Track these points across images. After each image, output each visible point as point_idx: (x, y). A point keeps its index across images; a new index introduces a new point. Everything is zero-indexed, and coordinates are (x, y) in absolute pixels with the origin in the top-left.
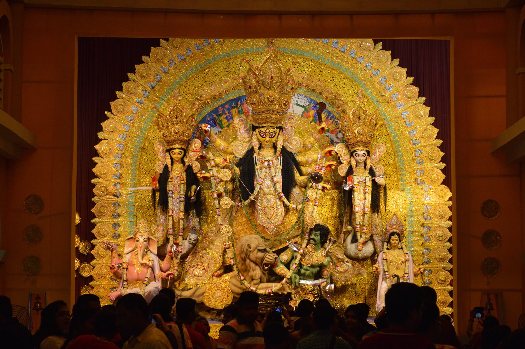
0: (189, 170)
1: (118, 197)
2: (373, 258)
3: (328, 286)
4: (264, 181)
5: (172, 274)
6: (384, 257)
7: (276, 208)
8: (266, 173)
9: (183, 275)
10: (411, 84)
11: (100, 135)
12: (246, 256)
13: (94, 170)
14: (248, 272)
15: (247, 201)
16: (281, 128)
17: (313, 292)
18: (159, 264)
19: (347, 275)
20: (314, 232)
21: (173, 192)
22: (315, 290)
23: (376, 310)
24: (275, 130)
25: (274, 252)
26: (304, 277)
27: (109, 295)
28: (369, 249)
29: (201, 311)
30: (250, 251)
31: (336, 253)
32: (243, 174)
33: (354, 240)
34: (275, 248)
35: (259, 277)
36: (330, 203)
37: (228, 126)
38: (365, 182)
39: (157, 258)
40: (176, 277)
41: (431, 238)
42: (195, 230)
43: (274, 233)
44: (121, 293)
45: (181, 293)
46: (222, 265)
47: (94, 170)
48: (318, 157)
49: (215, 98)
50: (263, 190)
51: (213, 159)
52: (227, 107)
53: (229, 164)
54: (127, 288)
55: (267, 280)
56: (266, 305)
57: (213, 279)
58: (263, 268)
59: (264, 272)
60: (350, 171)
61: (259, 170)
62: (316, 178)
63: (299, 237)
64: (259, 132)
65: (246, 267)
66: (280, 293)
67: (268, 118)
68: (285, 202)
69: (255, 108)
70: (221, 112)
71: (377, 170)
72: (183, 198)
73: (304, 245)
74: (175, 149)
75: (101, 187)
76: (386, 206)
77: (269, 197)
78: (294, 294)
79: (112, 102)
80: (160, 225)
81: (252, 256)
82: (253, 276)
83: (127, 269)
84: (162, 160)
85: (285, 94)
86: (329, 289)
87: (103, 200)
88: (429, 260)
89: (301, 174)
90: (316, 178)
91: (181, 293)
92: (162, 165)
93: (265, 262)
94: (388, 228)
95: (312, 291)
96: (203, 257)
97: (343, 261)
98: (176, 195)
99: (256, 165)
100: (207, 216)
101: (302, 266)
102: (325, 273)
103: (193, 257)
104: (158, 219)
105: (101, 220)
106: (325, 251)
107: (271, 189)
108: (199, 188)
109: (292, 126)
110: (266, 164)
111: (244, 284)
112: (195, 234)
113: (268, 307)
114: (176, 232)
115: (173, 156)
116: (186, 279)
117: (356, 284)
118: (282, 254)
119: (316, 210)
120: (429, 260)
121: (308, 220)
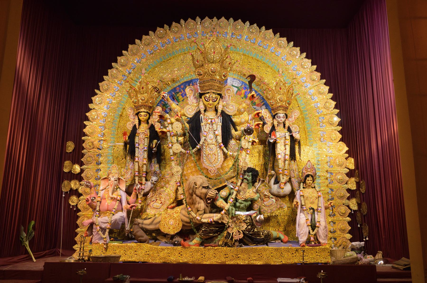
0: (152, 128)
1: (100, 150)
2: (292, 195)
3: (259, 216)
4: (207, 135)
5: (135, 206)
6: (302, 194)
7: (217, 155)
8: (210, 128)
9: (145, 207)
10: (314, 71)
11: (91, 106)
12: (193, 192)
13: (84, 130)
14: (194, 205)
15: (194, 149)
16: (220, 95)
17: (246, 221)
18: (127, 199)
19: (272, 208)
20: (247, 173)
21: (139, 144)
22: (247, 220)
23: (296, 236)
24: (217, 96)
25: (215, 189)
26: (239, 209)
27: (83, 223)
28: (287, 189)
29: (159, 236)
30: (196, 188)
31: (263, 191)
32: (192, 129)
33: (277, 182)
34: (216, 186)
35: (203, 209)
36: (257, 154)
37: (183, 101)
38: (285, 137)
39: (125, 193)
40: (139, 209)
41: (334, 181)
42: (156, 174)
43: (215, 175)
44: (93, 221)
45: (143, 222)
46: (175, 200)
47: (84, 130)
48: (249, 119)
49: (174, 81)
50: (207, 141)
51: (169, 119)
52: (183, 87)
53: (180, 118)
54: (98, 217)
55: (209, 211)
56: (209, 231)
57: (167, 211)
58: (207, 201)
59: (207, 205)
60: (273, 128)
61: (204, 126)
62: (249, 130)
63: (234, 178)
64: (204, 98)
65: (193, 200)
66: (220, 222)
67: (211, 85)
68: (224, 150)
69: (202, 78)
70: (178, 91)
71: (293, 129)
72: (147, 148)
73: (239, 184)
74: (142, 112)
75: (89, 142)
76: (300, 156)
77: (211, 146)
78: (231, 223)
79: (100, 83)
80: (129, 169)
81: (198, 192)
82: (198, 208)
83: (100, 202)
84: (132, 121)
85: (225, 68)
86: (259, 219)
87: (90, 152)
88: (332, 197)
89: (236, 130)
90: (249, 130)
91: (143, 222)
92: (132, 125)
93: (208, 196)
94: (304, 171)
95: (245, 220)
96: (161, 194)
97: (269, 197)
98: (141, 146)
99: (202, 122)
100: (166, 164)
101: (238, 200)
102: (256, 206)
103: (153, 193)
104: (127, 165)
105: (88, 167)
106: (255, 189)
107: (213, 141)
108: (159, 142)
109: (229, 96)
110: (210, 121)
111: (191, 215)
112: (156, 177)
113: (210, 233)
114: (141, 175)
115: (140, 118)
116: (148, 211)
117: (277, 216)
118: (222, 191)
119: (248, 157)
120: (332, 197)
121: (241, 164)
